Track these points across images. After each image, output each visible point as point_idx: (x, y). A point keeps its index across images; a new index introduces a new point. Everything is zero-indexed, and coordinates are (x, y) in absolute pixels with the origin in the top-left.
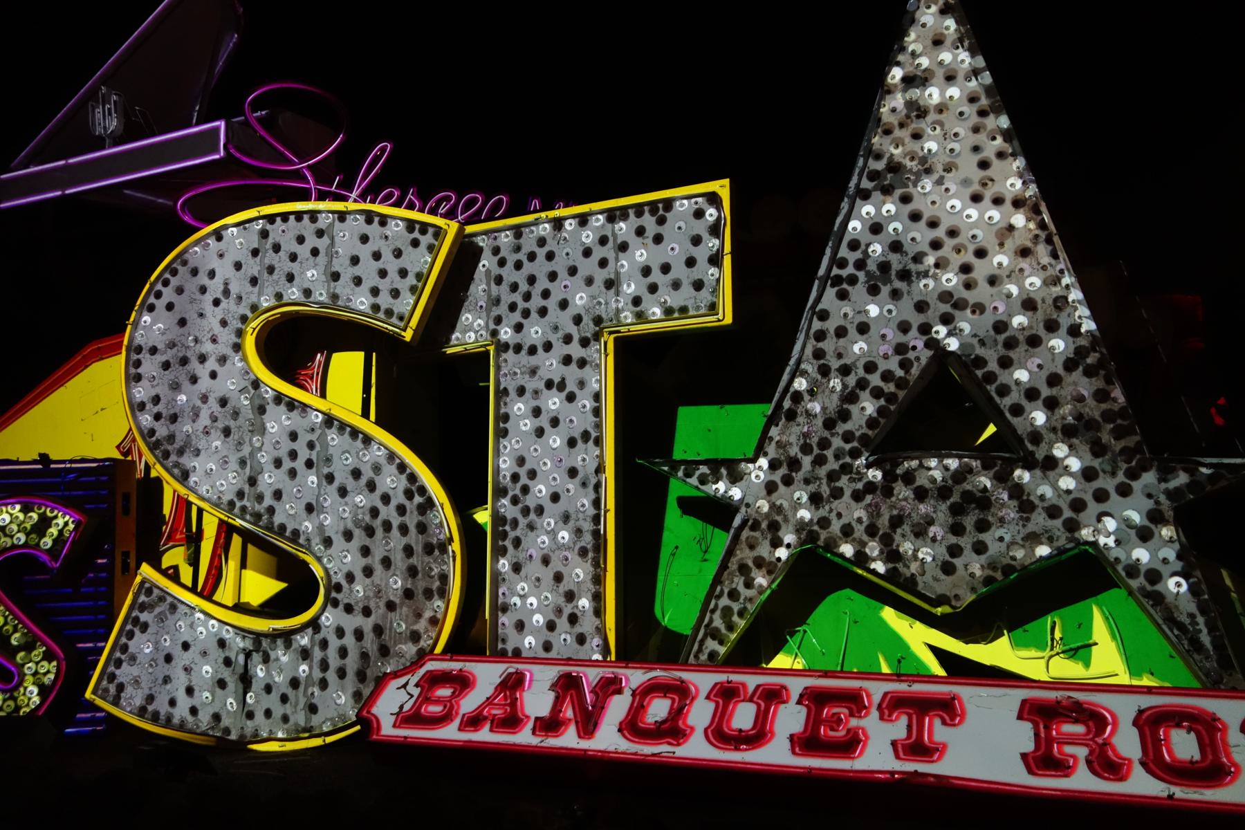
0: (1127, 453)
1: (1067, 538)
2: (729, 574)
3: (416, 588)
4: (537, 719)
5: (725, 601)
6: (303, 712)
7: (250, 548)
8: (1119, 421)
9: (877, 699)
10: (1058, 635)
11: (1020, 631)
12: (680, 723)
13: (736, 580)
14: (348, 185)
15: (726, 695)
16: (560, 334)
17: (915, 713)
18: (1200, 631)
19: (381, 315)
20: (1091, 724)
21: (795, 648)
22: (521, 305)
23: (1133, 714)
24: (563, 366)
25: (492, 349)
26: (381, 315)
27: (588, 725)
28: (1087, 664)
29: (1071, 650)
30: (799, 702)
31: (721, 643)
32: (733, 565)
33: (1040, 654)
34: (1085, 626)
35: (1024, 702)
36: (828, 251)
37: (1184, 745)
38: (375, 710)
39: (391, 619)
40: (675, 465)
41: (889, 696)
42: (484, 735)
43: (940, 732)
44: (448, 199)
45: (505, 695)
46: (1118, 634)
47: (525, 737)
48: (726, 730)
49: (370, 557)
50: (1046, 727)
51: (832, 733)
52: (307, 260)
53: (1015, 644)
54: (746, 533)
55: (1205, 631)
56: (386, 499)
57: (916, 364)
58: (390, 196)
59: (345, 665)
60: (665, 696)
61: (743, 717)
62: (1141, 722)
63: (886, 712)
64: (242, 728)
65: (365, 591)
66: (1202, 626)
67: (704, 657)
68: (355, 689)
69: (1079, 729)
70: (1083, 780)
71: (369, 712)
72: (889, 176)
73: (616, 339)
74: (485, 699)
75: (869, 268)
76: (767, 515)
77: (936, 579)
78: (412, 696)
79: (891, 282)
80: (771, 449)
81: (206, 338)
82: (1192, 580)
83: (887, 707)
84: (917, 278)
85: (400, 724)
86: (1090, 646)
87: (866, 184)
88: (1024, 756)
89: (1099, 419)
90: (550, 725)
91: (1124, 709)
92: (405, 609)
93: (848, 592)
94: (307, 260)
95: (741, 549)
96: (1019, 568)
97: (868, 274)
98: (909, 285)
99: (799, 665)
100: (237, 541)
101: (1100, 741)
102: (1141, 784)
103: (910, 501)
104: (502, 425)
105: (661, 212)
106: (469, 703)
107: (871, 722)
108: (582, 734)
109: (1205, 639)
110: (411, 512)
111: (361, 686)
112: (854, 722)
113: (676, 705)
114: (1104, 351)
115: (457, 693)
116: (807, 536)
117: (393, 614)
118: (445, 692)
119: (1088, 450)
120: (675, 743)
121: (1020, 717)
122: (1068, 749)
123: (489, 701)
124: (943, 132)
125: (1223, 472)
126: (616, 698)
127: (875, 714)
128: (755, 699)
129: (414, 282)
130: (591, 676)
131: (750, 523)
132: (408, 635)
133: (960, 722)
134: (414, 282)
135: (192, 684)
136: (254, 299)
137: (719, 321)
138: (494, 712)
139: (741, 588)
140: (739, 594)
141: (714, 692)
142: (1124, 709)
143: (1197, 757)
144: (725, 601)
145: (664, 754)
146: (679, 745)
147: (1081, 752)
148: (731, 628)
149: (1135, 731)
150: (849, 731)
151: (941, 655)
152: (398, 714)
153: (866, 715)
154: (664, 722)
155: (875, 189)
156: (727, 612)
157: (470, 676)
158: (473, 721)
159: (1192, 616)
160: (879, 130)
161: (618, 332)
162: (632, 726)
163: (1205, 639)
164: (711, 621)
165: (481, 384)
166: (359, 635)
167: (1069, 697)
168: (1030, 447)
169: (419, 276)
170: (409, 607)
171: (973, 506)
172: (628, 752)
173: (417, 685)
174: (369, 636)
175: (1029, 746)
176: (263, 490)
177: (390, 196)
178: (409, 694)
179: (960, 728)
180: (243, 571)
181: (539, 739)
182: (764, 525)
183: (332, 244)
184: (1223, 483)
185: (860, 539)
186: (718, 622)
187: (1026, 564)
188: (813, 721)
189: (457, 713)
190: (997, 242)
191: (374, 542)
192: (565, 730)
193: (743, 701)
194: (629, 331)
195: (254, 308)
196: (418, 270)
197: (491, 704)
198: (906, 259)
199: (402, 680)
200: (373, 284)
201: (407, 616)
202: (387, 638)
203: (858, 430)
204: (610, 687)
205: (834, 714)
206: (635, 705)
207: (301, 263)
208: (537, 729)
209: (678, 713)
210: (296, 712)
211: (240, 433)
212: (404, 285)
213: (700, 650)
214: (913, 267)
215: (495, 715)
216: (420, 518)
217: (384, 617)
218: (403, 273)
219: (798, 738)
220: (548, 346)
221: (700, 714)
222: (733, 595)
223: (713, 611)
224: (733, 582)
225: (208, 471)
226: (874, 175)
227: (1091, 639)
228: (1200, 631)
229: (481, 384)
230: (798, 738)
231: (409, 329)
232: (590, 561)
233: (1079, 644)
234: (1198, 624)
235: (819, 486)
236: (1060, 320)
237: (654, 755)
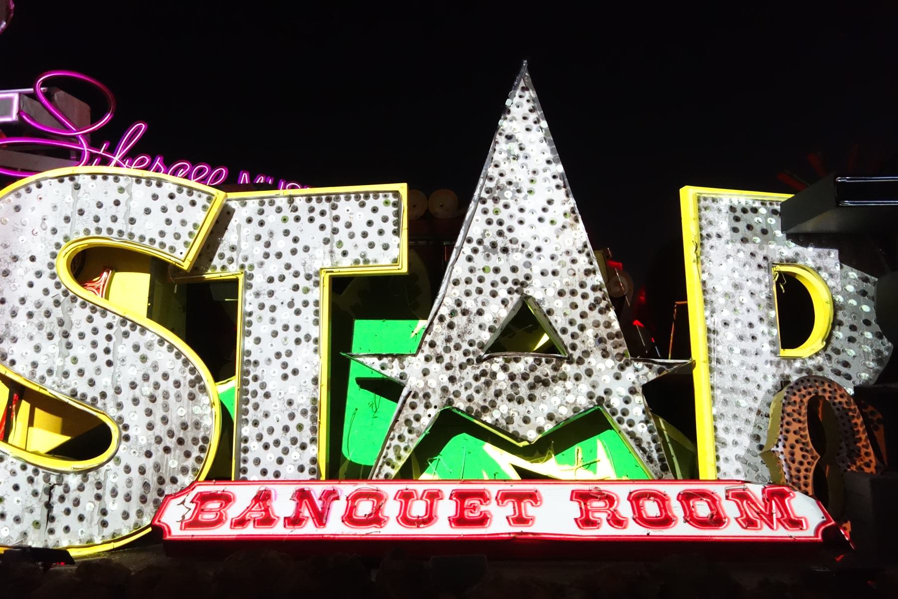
0: (620, 356)
1: (589, 402)
2: (399, 425)
3: (187, 437)
4: (285, 518)
5: (396, 442)
6: (97, 526)
7: (37, 411)
8: (616, 339)
9: (494, 495)
10: (580, 456)
11: (560, 455)
12: (380, 515)
13: (403, 428)
14: (112, 150)
15: (406, 497)
16: (292, 271)
17: (516, 501)
18: (652, 451)
19: (166, 250)
20: (607, 501)
21: (434, 469)
22: (579, 321)
23: (627, 495)
24: (293, 292)
25: (241, 278)
26: (166, 250)
27: (320, 518)
28: (595, 473)
29: (587, 464)
30: (451, 498)
31: (393, 467)
32: (402, 419)
33: (571, 467)
34: (593, 451)
35: (573, 492)
36: (462, 232)
37: (651, 509)
38: (163, 520)
39: (167, 459)
40: (352, 356)
41: (501, 492)
42: (250, 530)
43: (529, 509)
44: (184, 167)
45: (260, 505)
46: (611, 455)
47: (279, 530)
48: (409, 517)
49: (152, 416)
50: (585, 504)
51: (471, 515)
52: (111, 207)
53: (559, 462)
54: (410, 400)
55: (655, 451)
56: (165, 376)
57: (510, 302)
58: (143, 161)
59: (131, 491)
60: (368, 500)
61: (418, 509)
62: (631, 499)
63: (500, 501)
64: (46, 541)
65: (147, 440)
66: (653, 449)
67: (382, 477)
68: (138, 508)
69: (601, 504)
70: (606, 530)
71: (159, 521)
72: (497, 191)
73: (330, 276)
74: (245, 508)
75: (485, 244)
76: (423, 389)
77: (520, 426)
78: (190, 509)
79: (497, 253)
80: (426, 349)
81: (26, 257)
82: (649, 425)
83: (501, 499)
84: (512, 252)
85: (185, 528)
86: (596, 462)
87: (484, 195)
88: (576, 520)
89: (606, 337)
90: (295, 521)
91: (622, 492)
92: (178, 452)
93: (464, 435)
94: (111, 207)
95: (407, 410)
96: (564, 419)
97: (485, 248)
98: (507, 256)
99: (436, 477)
100: (25, 406)
101: (612, 509)
102: (634, 530)
103: (506, 381)
104: (246, 328)
105: (362, 199)
106: (234, 511)
107: (492, 508)
108: (318, 525)
109: (655, 455)
110: (185, 385)
111: (143, 505)
112: (483, 508)
113: (375, 505)
114: (609, 300)
115: (223, 505)
116: (447, 402)
117: (169, 455)
118: (214, 505)
119: (600, 353)
120: (379, 526)
121: (571, 499)
122: (597, 515)
123: (249, 509)
124: (527, 170)
125: (664, 367)
126: (336, 502)
127: (494, 502)
128: (424, 498)
129: (192, 229)
130: (317, 490)
131: (412, 394)
132: (180, 468)
133: (541, 504)
134: (192, 229)
135: (5, 510)
136: (67, 232)
137: (399, 269)
138: (253, 516)
139: (406, 434)
140: (404, 437)
141: (398, 495)
142: (622, 492)
143: (659, 514)
144: (396, 442)
145: (373, 534)
146: (381, 527)
147: (603, 516)
148: (399, 458)
149: (629, 503)
150: (481, 512)
151: (519, 470)
152: (182, 522)
153: (490, 503)
154: (370, 515)
155: (489, 198)
156: (397, 448)
157: (231, 494)
158: (241, 522)
159: (649, 443)
160: (492, 164)
161: (332, 272)
162: (349, 518)
163: (655, 455)
164: (387, 454)
165: (226, 300)
166: (142, 471)
167: (596, 488)
168: (571, 351)
169: (195, 226)
170: (180, 450)
171: (541, 384)
172: (350, 533)
173: (192, 502)
174: (150, 471)
175: (578, 515)
176: (69, 369)
177: (143, 161)
178: (187, 508)
179: (541, 507)
180: (30, 428)
181: (290, 530)
182: (421, 395)
183: (131, 198)
184: (665, 373)
185: (478, 403)
186: (391, 455)
187: (568, 417)
188: (461, 509)
189: (226, 518)
190: (555, 235)
191: (156, 405)
192: (306, 524)
193: (417, 499)
194: (339, 272)
195: (66, 238)
196: (194, 222)
197: (250, 511)
198: (506, 240)
199: (181, 499)
200: (94, 214)
201: (179, 456)
202: (164, 472)
203: (477, 339)
204: (332, 496)
205: (471, 504)
206: (350, 505)
207: (106, 209)
208: (287, 524)
209: (377, 510)
210: (91, 527)
211: (52, 328)
212: (184, 232)
213: (379, 472)
214: (510, 246)
215: (255, 518)
216: (191, 389)
217: (162, 457)
218: (184, 223)
219: (453, 519)
220: (282, 278)
221: (391, 509)
222: (401, 438)
223: (388, 448)
224: (401, 429)
225: (24, 354)
226: (488, 191)
227: (596, 457)
228: (652, 451)
229: (226, 300)
230: (453, 519)
231: (186, 261)
232: (309, 418)
233: (591, 461)
234: (651, 447)
235: (454, 371)
236: (587, 282)
237: (367, 534)
